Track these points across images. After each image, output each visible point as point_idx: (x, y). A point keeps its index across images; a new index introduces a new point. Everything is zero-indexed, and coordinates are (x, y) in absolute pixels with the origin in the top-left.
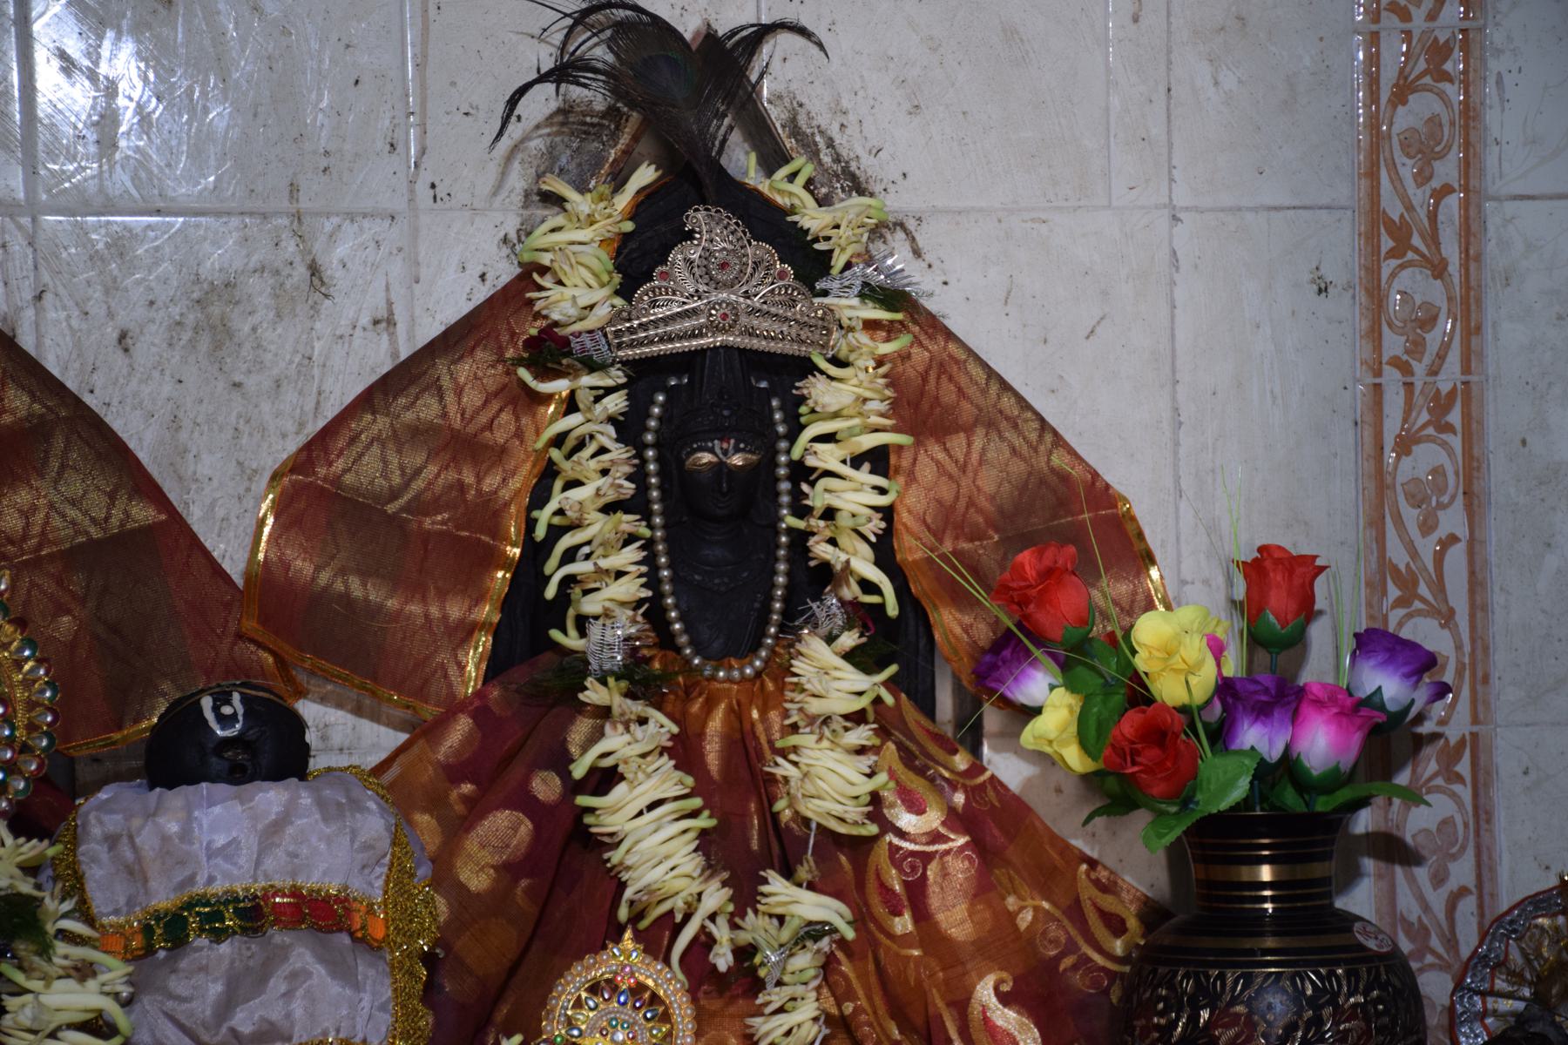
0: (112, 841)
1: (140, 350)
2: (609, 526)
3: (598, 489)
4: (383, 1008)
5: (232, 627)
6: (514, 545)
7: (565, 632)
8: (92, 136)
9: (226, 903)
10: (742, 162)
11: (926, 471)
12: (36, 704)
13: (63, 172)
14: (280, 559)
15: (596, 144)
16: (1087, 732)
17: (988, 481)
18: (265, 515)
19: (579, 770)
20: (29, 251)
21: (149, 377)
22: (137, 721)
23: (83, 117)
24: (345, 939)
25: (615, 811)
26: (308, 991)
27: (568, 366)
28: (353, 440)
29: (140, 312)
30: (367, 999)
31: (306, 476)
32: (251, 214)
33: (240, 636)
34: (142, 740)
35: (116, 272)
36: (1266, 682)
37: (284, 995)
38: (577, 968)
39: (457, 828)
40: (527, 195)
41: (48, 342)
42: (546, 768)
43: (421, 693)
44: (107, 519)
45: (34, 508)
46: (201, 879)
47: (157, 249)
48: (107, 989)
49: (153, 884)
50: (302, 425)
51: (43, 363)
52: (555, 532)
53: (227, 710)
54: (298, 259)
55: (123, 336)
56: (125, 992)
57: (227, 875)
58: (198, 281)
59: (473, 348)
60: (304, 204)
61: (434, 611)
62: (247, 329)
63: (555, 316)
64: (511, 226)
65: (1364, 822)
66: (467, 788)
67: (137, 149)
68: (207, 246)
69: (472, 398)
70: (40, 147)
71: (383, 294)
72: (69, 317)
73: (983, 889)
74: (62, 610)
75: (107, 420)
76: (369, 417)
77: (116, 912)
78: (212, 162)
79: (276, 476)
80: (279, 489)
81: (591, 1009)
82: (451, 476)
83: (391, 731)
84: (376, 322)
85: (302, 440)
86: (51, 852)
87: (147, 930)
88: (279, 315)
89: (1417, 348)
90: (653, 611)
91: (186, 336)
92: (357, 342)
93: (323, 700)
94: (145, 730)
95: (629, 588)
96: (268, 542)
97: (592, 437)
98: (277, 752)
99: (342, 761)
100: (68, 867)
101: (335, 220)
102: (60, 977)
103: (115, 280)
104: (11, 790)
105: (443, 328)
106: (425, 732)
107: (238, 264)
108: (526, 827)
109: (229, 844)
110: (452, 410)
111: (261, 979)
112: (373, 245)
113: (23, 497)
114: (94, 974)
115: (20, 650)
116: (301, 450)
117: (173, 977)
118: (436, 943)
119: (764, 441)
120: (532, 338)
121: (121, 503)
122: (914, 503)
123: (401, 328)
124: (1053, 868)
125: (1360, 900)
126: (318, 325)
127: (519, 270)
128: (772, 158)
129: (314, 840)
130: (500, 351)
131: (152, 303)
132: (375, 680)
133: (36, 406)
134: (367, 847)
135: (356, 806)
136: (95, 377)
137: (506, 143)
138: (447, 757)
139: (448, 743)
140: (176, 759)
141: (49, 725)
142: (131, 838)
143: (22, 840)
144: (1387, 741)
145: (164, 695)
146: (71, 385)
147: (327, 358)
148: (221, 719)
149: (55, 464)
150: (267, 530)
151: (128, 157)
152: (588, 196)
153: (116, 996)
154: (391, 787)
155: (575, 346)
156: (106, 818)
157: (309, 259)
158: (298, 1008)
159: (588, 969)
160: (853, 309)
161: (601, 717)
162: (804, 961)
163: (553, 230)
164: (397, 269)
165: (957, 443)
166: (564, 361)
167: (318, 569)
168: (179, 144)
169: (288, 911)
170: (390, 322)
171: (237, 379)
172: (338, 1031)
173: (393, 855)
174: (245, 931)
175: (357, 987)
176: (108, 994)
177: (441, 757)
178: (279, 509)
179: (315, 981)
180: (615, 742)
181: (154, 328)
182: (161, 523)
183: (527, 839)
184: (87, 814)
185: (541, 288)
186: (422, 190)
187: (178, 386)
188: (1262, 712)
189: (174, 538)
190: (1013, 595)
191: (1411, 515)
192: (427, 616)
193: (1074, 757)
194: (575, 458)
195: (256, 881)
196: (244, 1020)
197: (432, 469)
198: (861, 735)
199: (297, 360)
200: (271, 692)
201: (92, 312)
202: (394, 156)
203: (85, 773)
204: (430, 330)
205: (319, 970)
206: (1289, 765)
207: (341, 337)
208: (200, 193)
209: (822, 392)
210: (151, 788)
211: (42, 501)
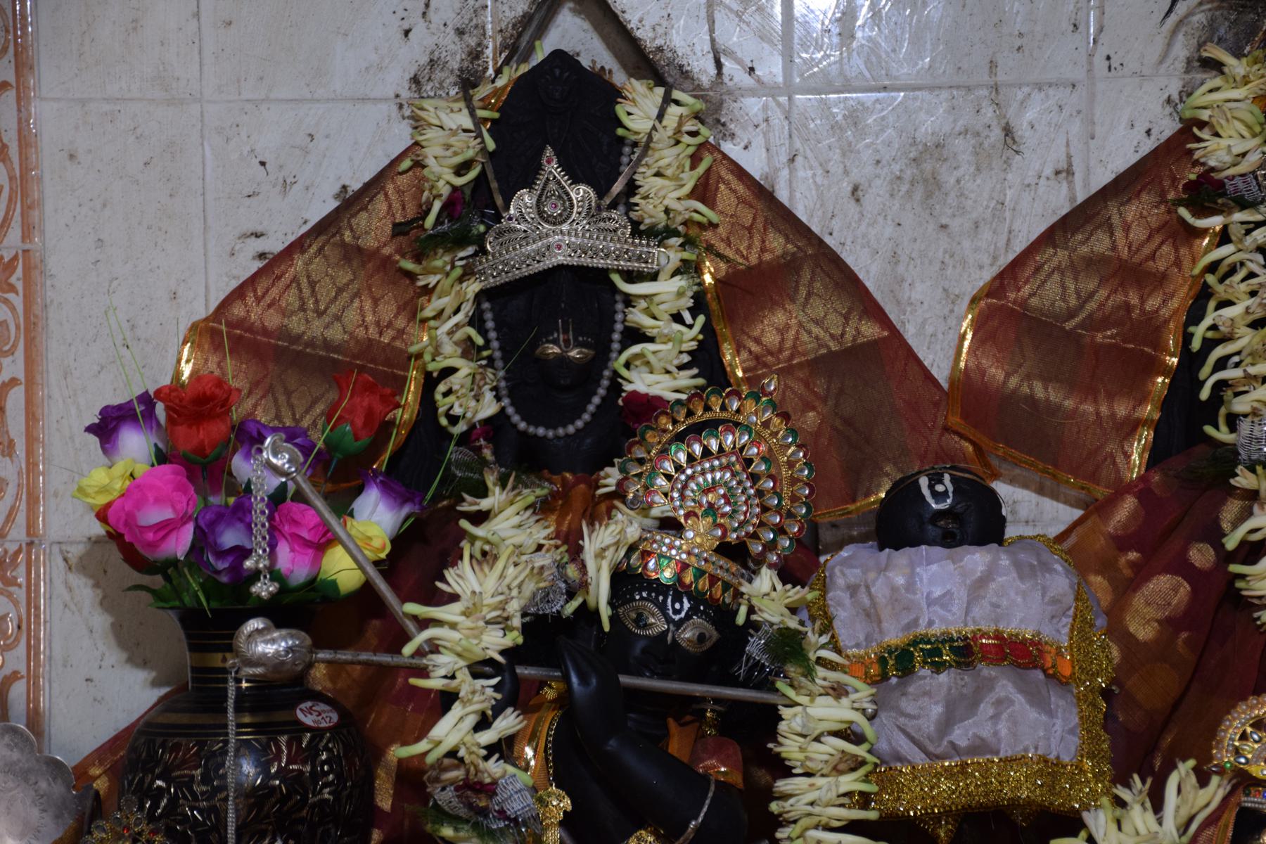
0: (853, 590)
1: (869, 200)
2: (1257, 339)
3: (1247, 308)
4: (1072, 731)
5: (940, 421)
6: (1172, 355)
7: (1217, 428)
8: (835, 30)
9: (944, 642)
12: (798, 480)
13: (813, 59)
14: (977, 366)
15: (1252, 16)
18: (965, 332)
19: (1231, 543)
20: (786, 123)
21: (875, 222)
22: (867, 495)
23: (829, 15)
24: (1040, 675)
26: (1010, 716)
27: (1223, 205)
28: (1038, 269)
29: (869, 169)
30: (1059, 722)
31: (999, 299)
32: (958, 87)
33: (946, 429)
34: (870, 512)
35: (851, 138)
37: (992, 718)
38: (1242, 707)
39: (1126, 588)
40: (1189, 61)
41: (798, 195)
42: (1202, 541)
43: (1094, 477)
44: (842, 335)
45: (787, 327)
46: (923, 622)
47: (883, 118)
48: (856, 705)
49: (885, 625)
50: (995, 258)
51: (795, 212)
52: (1209, 345)
53: (940, 488)
54: (994, 123)
55: (855, 189)
56: (870, 709)
57: (943, 620)
58: (914, 143)
59: (1140, 192)
60: (1001, 77)
61: (1104, 410)
62: (952, 181)
63: (1212, 163)
64: (1174, 89)
66: (1133, 555)
67: (870, 39)
68: (922, 116)
69: (1138, 234)
70: (796, 40)
71: (1064, 149)
72: (814, 175)
74: (809, 407)
75: (842, 256)
76: (1051, 251)
77: (858, 646)
78: (928, 46)
79: (974, 300)
80: (977, 311)
81: (1256, 742)
82: (1120, 298)
83: (1068, 508)
84: (1057, 173)
85: (995, 271)
86: (810, 596)
87: (882, 661)
88: (978, 169)
91: (904, 188)
92: (1041, 190)
93: (1012, 481)
94: (873, 503)
96: (968, 353)
97: (1242, 264)
98: (979, 523)
99: (1029, 531)
100: (819, 609)
101: (1026, 90)
102: (821, 695)
103: (850, 144)
104: (779, 547)
105: (1113, 176)
106: (1096, 509)
107: (947, 128)
108: (1185, 588)
109: (944, 595)
110: (1121, 243)
111: (973, 705)
112: (1057, 109)
113: (779, 318)
114: (847, 694)
115: (785, 437)
116: (994, 279)
117: (904, 699)
118: (1113, 681)
120: (1191, 181)
121: (853, 322)
123: (1078, 178)
126: (1010, 176)
127: (1180, 126)
129: (1012, 594)
130: (1163, 194)
131: (878, 162)
132: (1056, 466)
133: (790, 246)
134: (1054, 601)
135: (1046, 568)
136: (833, 222)
137: (1173, 18)
138: (1116, 529)
139: (1118, 518)
140: (898, 527)
141: (806, 497)
142: (868, 588)
143: (789, 586)
145: (887, 475)
146: (815, 229)
147: (1016, 203)
148: (935, 494)
149: (803, 292)
150: (967, 344)
151: (862, 45)
152: (1244, 60)
153: (864, 711)
154: (1069, 552)
155: (1229, 188)
156: (847, 571)
157: (1003, 122)
158: (1003, 728)
159: (1252, 708)
161: (1249, 500)
163: (1211, 91)
164: (1076, 128)
166: (1220, 201)
167: (1008, 375)
168: (902, 33)
169: (993, 650)
170: (1070, 172)
171: (944, 222)
172: (1036, 748)
173: (1076, 608)
174: (959, 665)
175: (1051, 714)
176: (857, 710)
177: (1111, 529)
178: (977, 326)
179: (1017, 707)
181: (878, 182)
182: (884, 339)
183: (1186, 599)
184: (834, 567)
185: (1200, 140)
186: (1100, 62)
187: (898, 228)
189: (893, 350)
192: (1098, 414)
194: (1227, 282)
195: (966, 625)
196: (961, 735)
197: (1103, 293)
199: (992, 206)
200: (971, 473)
201: (832, 171)
202: (1076, 35)
203: (826, 536)
204: (1102, 177)
205: (1019, 698)
207: (1029, 185)
208: (918, 72)
210: (881, 549)
211: (794, 321)
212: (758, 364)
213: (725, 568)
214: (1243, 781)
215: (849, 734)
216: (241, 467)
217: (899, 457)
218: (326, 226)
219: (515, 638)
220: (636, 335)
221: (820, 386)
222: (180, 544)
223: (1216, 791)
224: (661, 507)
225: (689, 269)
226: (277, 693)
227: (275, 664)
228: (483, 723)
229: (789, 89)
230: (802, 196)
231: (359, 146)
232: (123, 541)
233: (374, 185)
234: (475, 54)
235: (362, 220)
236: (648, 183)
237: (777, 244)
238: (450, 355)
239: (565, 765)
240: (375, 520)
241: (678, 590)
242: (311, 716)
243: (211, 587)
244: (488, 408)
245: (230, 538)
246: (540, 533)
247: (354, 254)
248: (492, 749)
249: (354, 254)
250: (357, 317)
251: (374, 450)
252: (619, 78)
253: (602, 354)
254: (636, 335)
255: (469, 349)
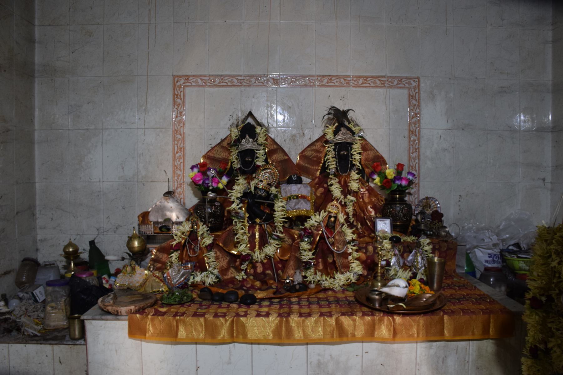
10: (346, 123)
11: (364, 155)
16: (381, 182)
17: (371, 156)
19: (329, 184)
25: (332, 188)
36: (399, 176)
39: (316, 190)
65: (407, 191)
69: (319, 146)
73: (369, 197)
89: (414, 143)
90: (336, 168)
95: (334, 166)
98: (299, 181)
106: (313, 180)
119: (348, 151)
122: (363, 158)
124: (376, 195)
125: (406, 199)
128: (349, 123)
140: (290, 182)
144: (410, 183)
160: (357, 138)
162: (351, 204)
164: (311, 133)
165: (368, 152)
180: (333, 181)
188: (398, 180)
189: (289, 160)
190: (373, 167)
191: (413, 160)
193: (379, 184)
196: (296, 207)
198: (357, 181)
204: (315, 140)
206: (401, 185)
209: (354, 146)
212: (272, 162)
213: (268, 186)
214: (330, 212)
215: (283, 207)
216: (208, 173)
217: (289, 173)
218: (219, 144)
219: (242, 195)
220: (257, 157)
221: (280, 164)
222: (201, 182)
223: (326, 213)
224: (260, 179)
225: (264, 149)
226: (213, 201)
227: (212, 197)
228: (238, 205)
229: (277, 128)
230: (278, 141)
231: (224, 134)
232: (194, 182)
233: (225, 139)
234: (238, 123)
235: (224, 143)
236: (259, 139)
237: (275, 146)
238: (234, 160)
239: (248, 210)
240: (225, 180)
241: (262, 189)
242: (217, 204)
243: (205, 188)
244: (239, 166)
245: (207, 182)
246: (245, 182)
247: (223, 147)
248: (239, 208)
249: (223, 147)
250: (223, 155)
251: (225, 172)
252: (256, 126)
253: (253, 160)
254: (257, 157)
255: (237, 159)
